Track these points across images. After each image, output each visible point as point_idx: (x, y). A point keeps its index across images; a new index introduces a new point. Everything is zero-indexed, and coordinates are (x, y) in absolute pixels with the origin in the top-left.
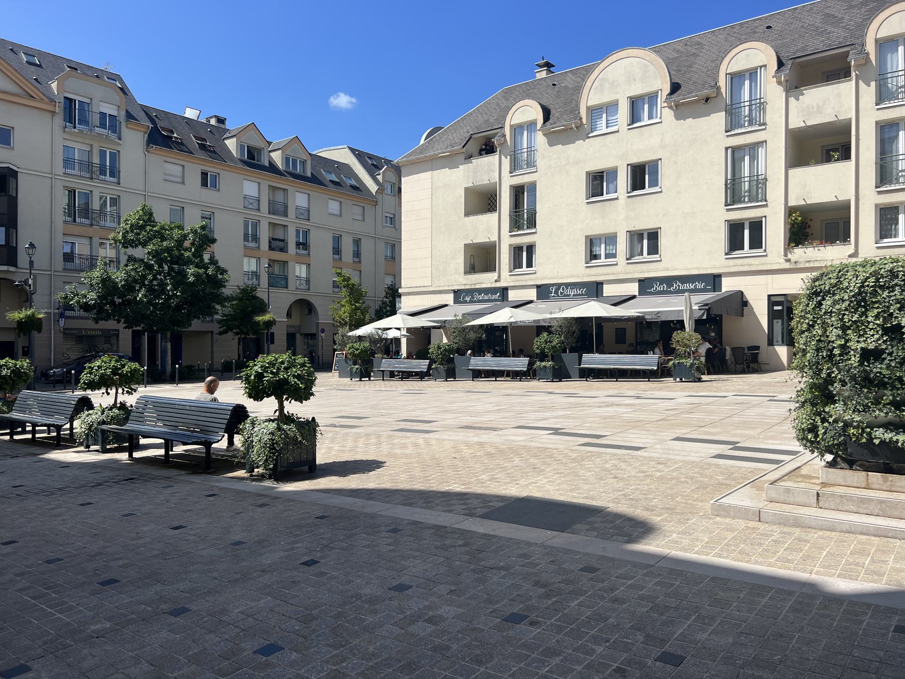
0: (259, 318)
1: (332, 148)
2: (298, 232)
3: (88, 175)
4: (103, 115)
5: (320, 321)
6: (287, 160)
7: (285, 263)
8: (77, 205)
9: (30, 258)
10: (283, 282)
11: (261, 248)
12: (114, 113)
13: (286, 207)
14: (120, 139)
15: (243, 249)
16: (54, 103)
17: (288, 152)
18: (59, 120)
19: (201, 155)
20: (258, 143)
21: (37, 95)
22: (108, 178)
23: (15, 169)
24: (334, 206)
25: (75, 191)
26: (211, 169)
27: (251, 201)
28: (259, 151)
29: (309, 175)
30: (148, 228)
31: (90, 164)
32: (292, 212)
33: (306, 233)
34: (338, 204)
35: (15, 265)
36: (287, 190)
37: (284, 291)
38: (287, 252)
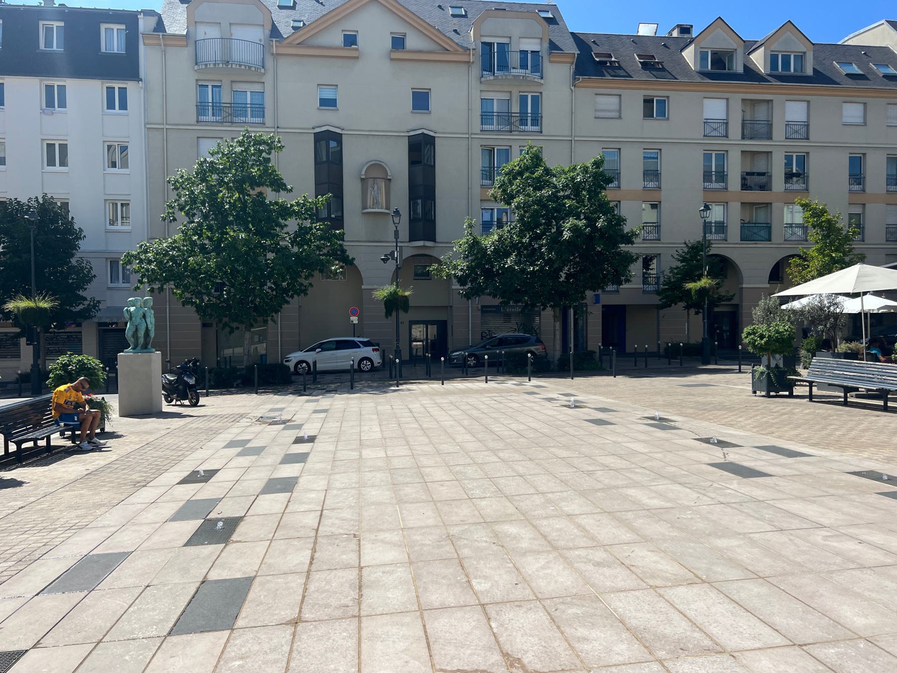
0: (690, 285)
1: (862, 31)
2: (789, 159)
3: (507, 128)
4: (524, 53)
5: (744, 286)
6: (773, 60)
7: (768, 205)
8: (496, 166)
9: (396, 227)
10: (763, 233)
11: (729, 189)
12: (536, 48)
13: (770, 126)
14: (542, 78)
15: (702, 193)
16: (468, 52)
17: (775, 47)
18: (476, 70)
19: (645, 76)
20: (725, 43)
21: (450, 46)
22: (529, 128)
23: (432, 134)
24: (852, 112)
25: (494, 149)
26: (657, 93)
27: (715, 126)
28: (730, 54)
29: (809, 72)
30: (527, 174)
31: (509, 115)
32: (778, 132)
33: (803, 160)
34: (860, 107)
35: (433, 240)
36: (772, 101)
37: (766, 244)
38: (771, 190)
